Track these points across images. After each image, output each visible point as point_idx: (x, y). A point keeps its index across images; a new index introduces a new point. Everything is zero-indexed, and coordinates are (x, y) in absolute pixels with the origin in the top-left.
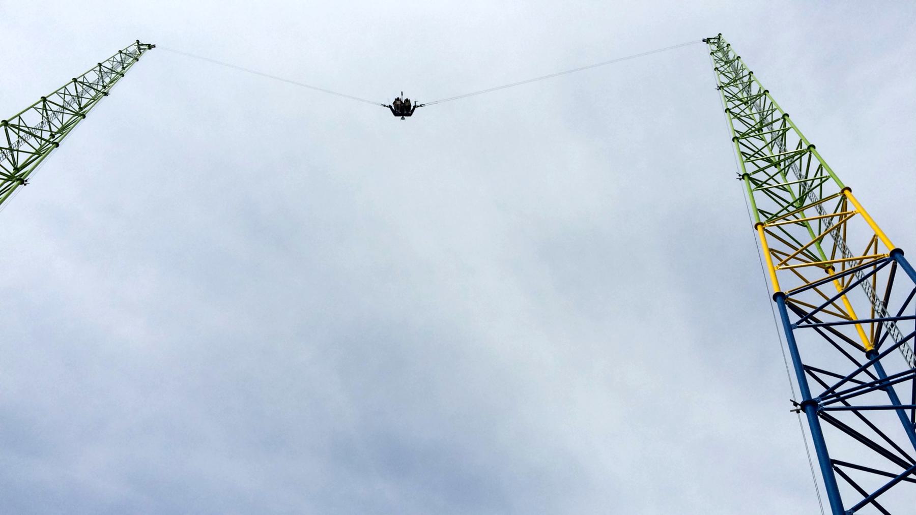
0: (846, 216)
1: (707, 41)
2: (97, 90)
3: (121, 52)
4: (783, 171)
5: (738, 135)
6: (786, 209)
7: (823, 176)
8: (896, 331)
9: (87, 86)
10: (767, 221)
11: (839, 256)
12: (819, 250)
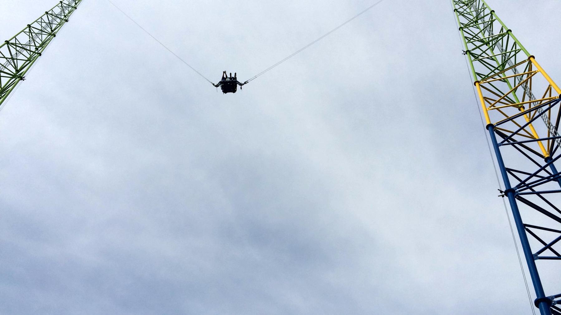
0: (531, 74)
2: (61, 19)
4: (491, 48)
5: (462, 26)
6: (493, 71)
7: (517, 49)
9: (55, 16)
11: (527, 99)
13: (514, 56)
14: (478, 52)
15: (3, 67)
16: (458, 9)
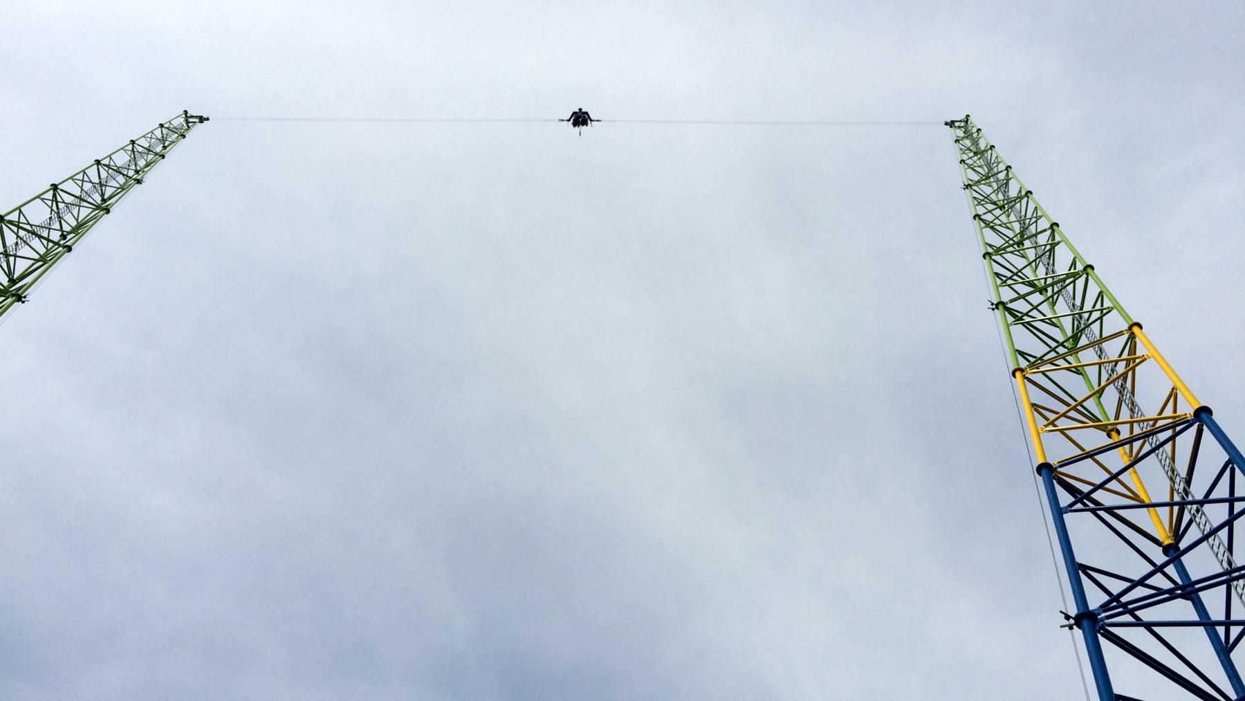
0: (1134, 361)
1: (951, 124)
2: (127, 176)
3: (162, 126)
4: (1051, 299)
5: (990, 250)
7: (1104, 307)
11: (1125, 415)
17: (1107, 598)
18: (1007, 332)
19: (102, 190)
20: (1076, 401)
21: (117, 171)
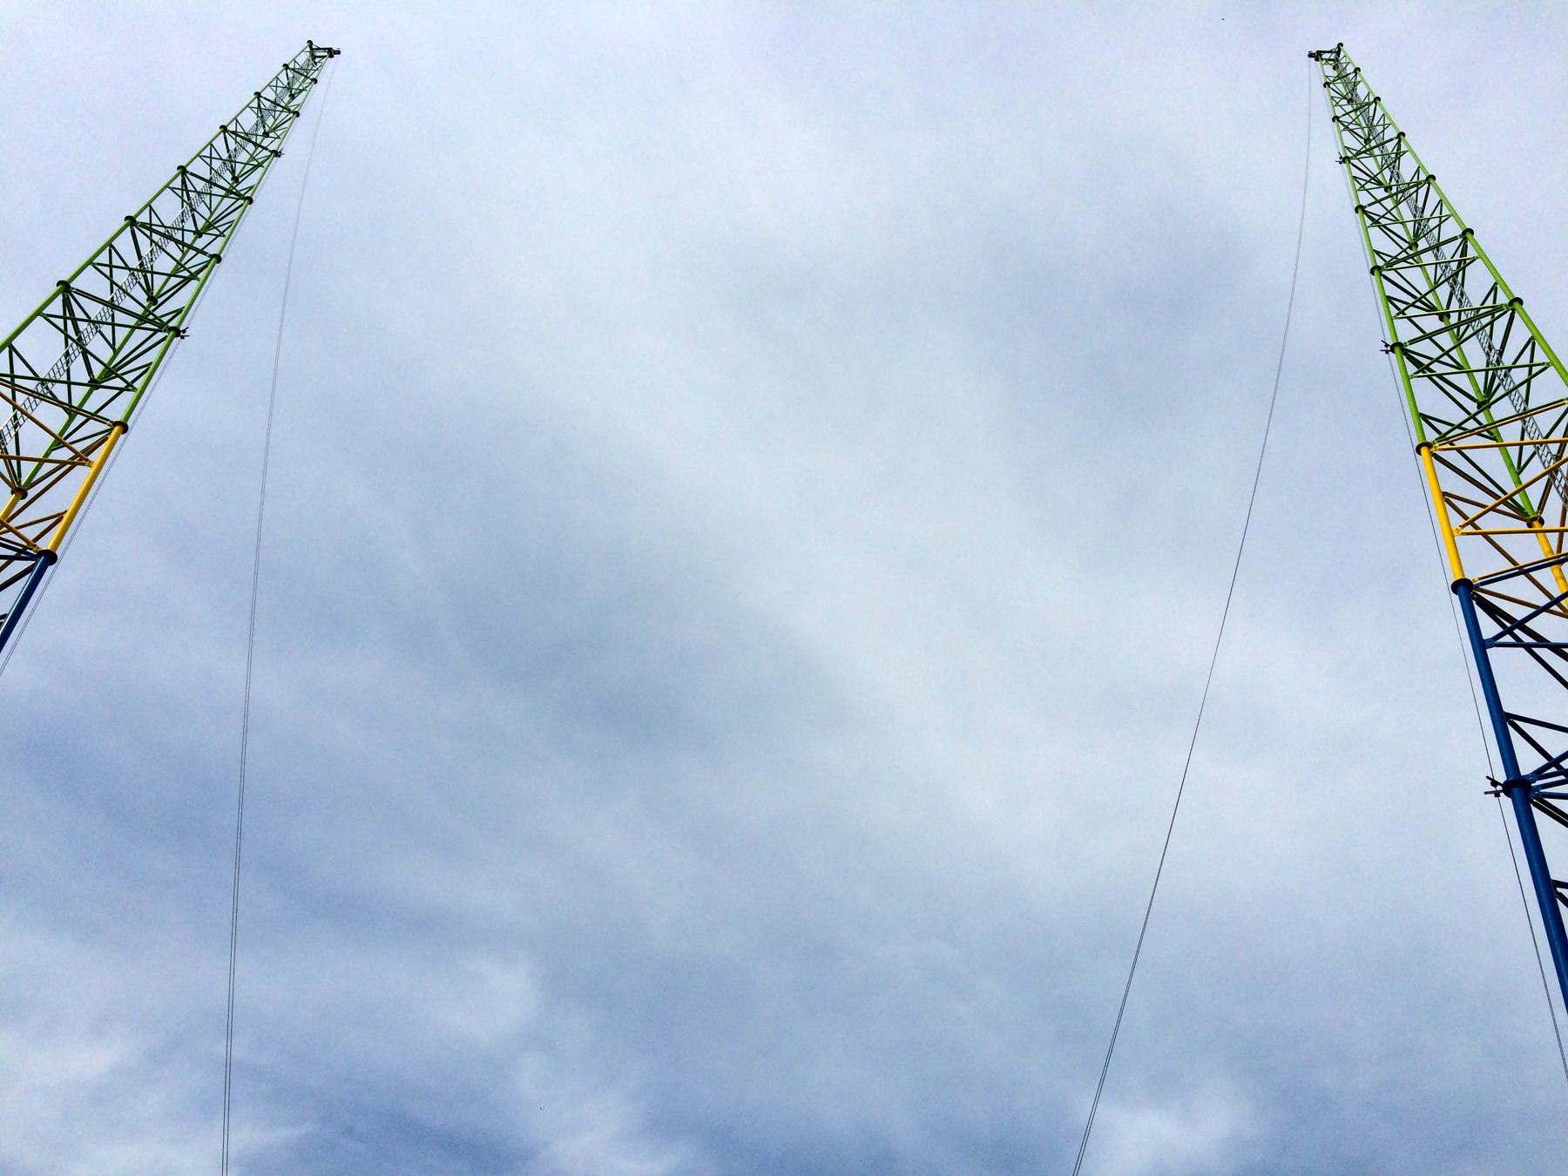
0: (1465, 262)
1: (1317, 56)
3: (286, 66)
4: (1395, 197)
5: (1380, 263)
6: (1405, 251)
7: (1443, 214)
8: (1509, 380)
9: (242, 138)
10: (1438, 440)
11: (1394, 182)
12: (1561, 581)
13: (1525, 385)
14: (1377, 209)
15: (121, 291)
16: (1366, 207)
17: (1544, 761)
18: (1407, 386)
19: (232, 166)
20: (1505, 493)
21: (246, 139)
